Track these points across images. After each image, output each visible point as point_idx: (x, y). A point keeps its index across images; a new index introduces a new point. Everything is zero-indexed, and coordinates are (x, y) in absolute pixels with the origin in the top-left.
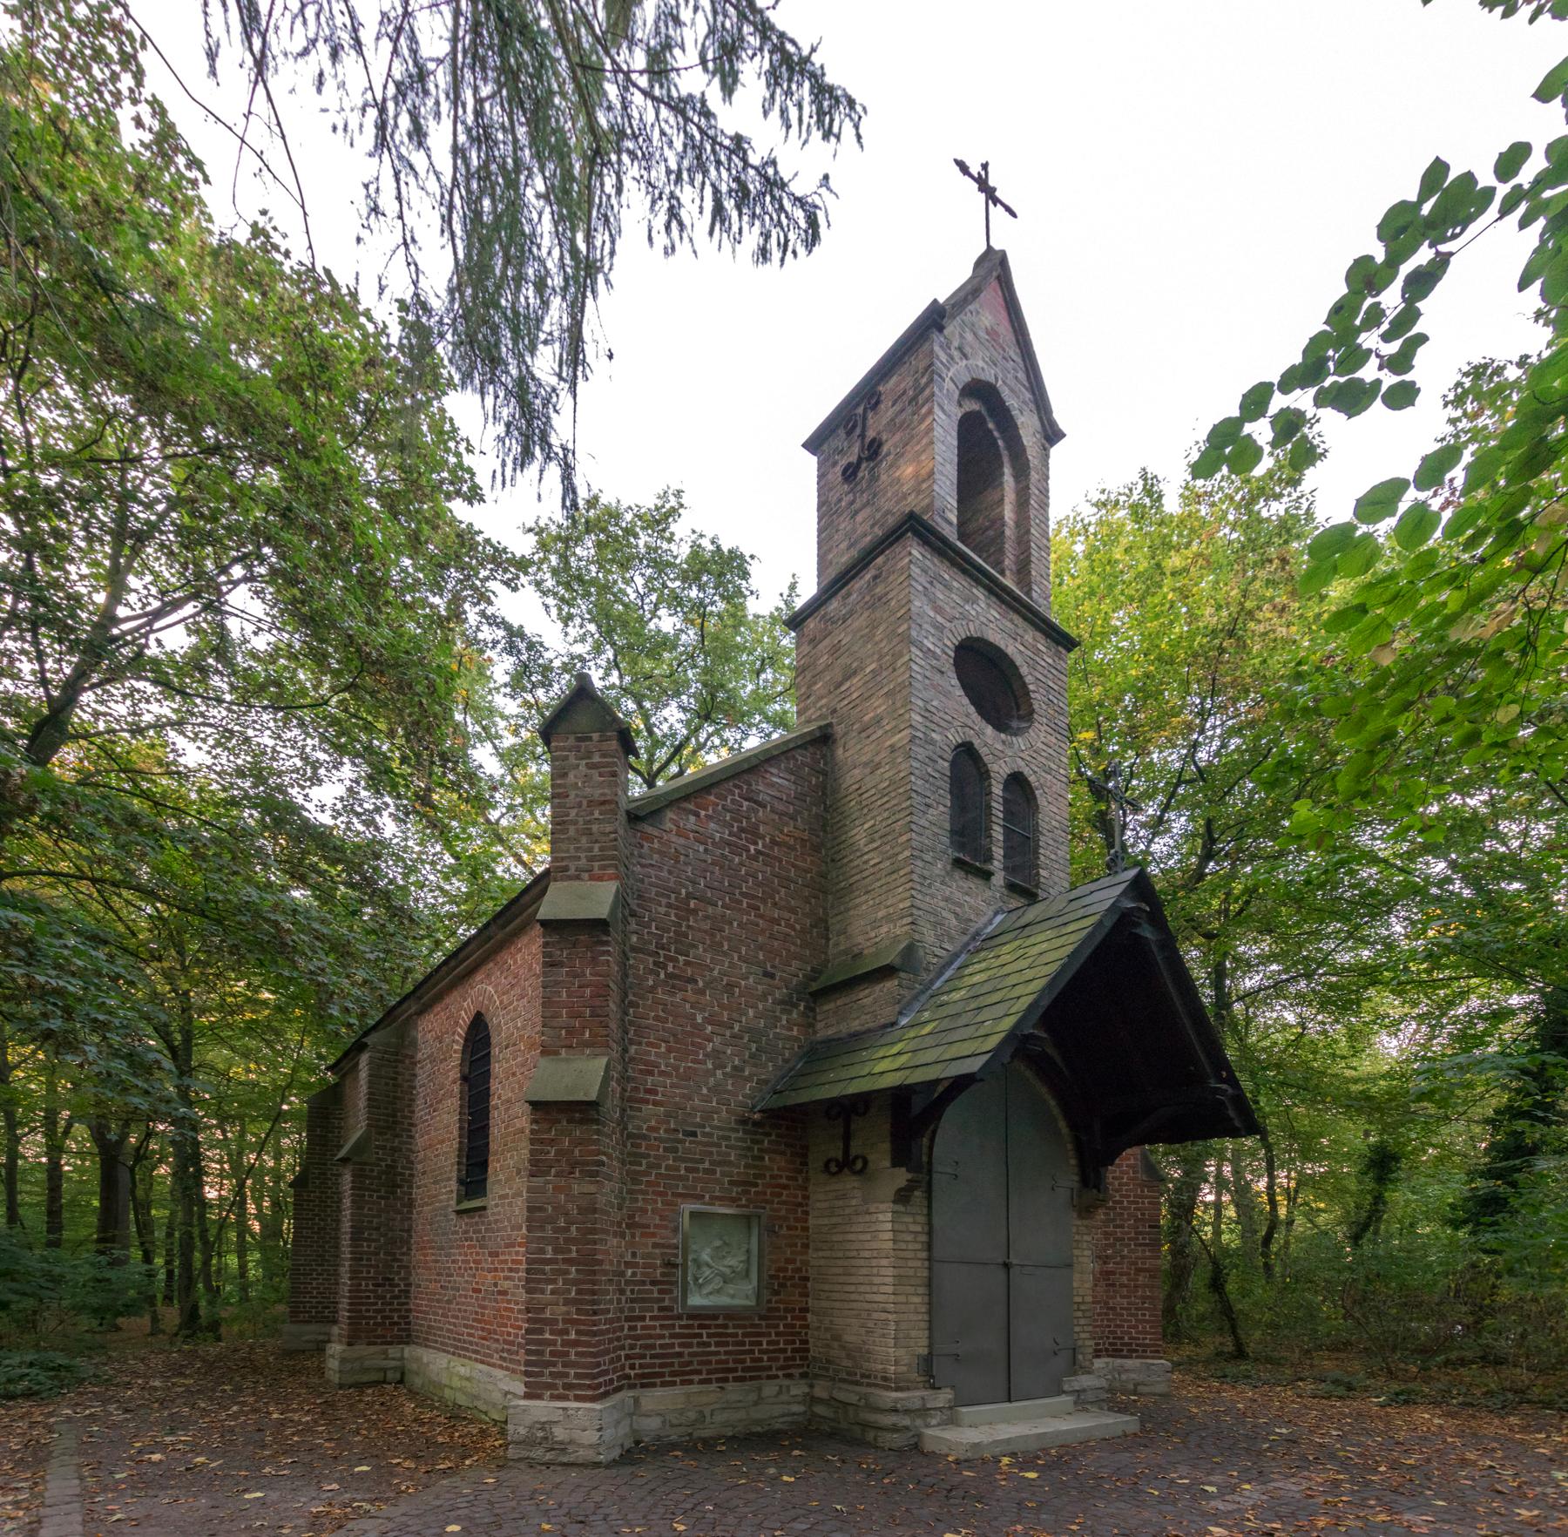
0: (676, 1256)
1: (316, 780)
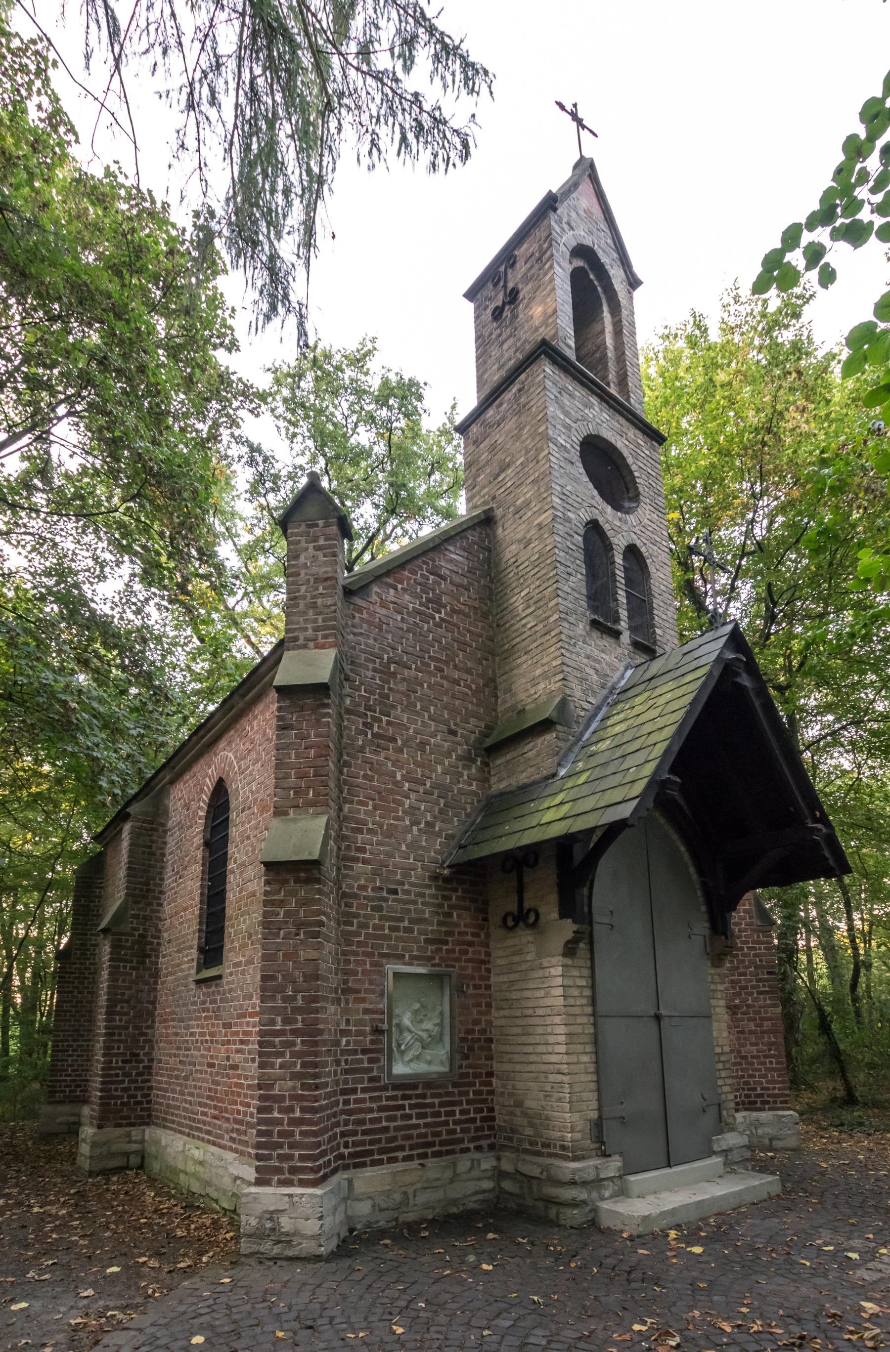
0: (383, 1022)
1: (102, 578)
